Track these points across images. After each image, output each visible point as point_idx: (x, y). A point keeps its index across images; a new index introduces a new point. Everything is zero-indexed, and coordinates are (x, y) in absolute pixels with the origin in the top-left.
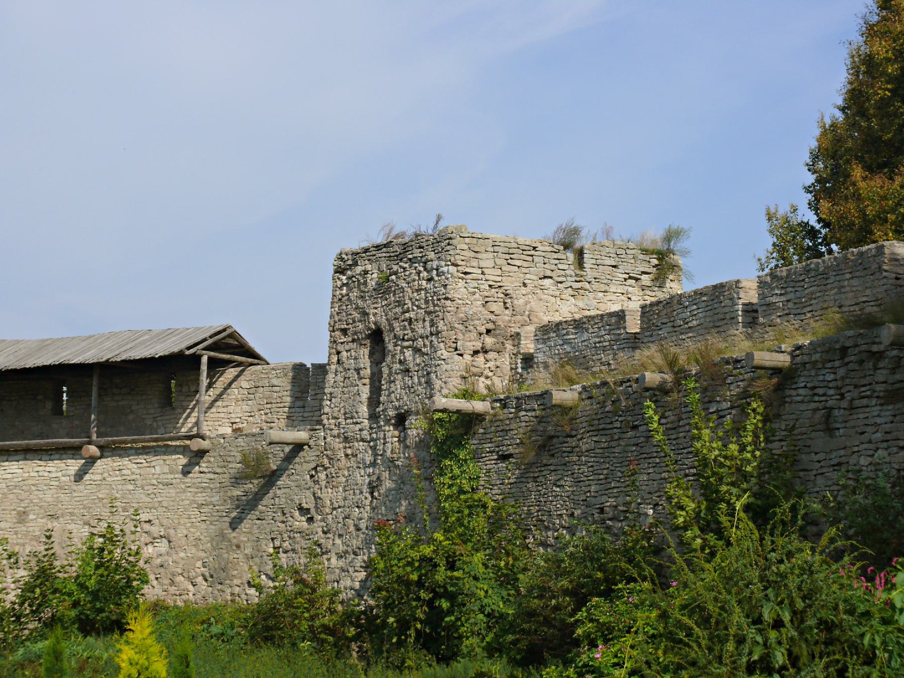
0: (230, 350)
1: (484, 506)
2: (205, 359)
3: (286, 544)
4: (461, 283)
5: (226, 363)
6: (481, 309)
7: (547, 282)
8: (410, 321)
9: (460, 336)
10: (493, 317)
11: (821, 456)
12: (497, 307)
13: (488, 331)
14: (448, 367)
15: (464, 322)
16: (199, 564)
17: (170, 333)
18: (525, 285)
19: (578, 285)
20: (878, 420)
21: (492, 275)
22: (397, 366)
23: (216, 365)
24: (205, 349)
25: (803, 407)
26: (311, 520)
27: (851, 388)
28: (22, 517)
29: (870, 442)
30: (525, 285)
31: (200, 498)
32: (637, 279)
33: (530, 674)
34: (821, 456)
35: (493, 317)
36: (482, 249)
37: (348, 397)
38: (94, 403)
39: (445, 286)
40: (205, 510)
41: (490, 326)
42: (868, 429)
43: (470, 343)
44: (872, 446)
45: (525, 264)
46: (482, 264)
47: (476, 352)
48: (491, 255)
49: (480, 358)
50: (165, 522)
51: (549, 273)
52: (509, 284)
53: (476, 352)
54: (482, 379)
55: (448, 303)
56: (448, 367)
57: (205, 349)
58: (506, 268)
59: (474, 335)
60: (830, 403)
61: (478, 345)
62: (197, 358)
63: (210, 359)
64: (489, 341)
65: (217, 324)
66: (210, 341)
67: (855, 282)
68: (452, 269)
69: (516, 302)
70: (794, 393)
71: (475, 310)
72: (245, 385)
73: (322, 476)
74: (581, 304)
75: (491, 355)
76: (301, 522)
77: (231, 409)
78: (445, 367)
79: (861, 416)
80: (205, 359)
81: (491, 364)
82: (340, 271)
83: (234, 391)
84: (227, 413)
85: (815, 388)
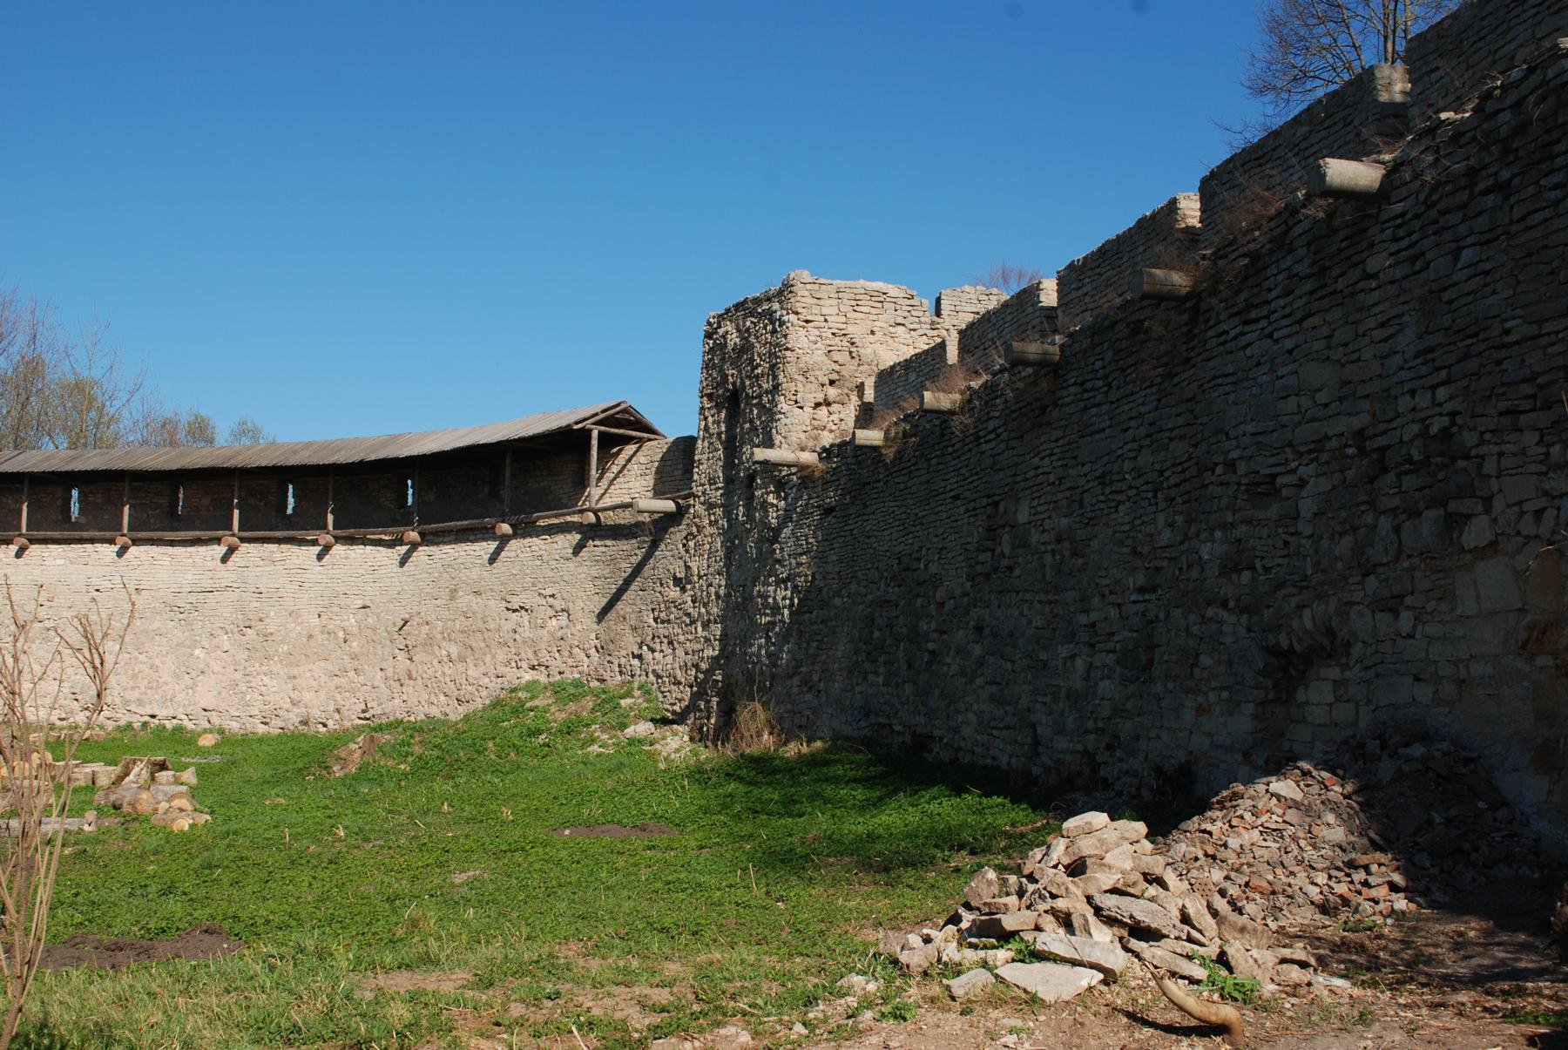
0: (623, 428)
2: (595, 434)
3: (663, 615)
4: (802, 332)
5: (627, 440)
6: (824, 358)
8: (757, 377)
9: (800, 387)
10: (837, 367)
12: (843, 357)
13: (832, 383)
14: (788, 421)
15: (804, 374)
16: (593, 636)
18: (873, 333)
20: (1143, 409)
21: (836, 321)
22: (747, 426)
23: (610, 444)
24: (596, 423)
26: (683, 590)
27: (1117, 374)
30: (873, 333)
35: (837, 367)
36: (824, 295)
37: (709, 463)
39: (785, 336)
41: (834, 377)
42: (1133, 423)
43: (810, 394)
44: (1135, 445)
45: (874, 311)
46: (825, 311)
47: (818, 405)
48: (835, 302)
49: (824, 410)
50: (566, 595)
51: (900, 320)
53: (818, 405)
54: (826, 433)
55: (788, 353)
56: (788, 421)
57: (596, 423)
58: (851, 315)
61: (820, 398)
62: (587, 433)
63: (601, 434)
64: (832, 392)
66: (602, 416)
68: (792, 317)
69: (862, 351)
70: (1065, 393)
71: (815, 358)
72: (643, 460)
73: (691, 544)
75: (834, 407)
76: (674, 593)
77: (631, 485)
78: (784, 421)
79: (1126, 408)
80: (595, 434)
81: (835, 417)
82: (709, 336)
83: (634, 468)
84: (628, 485)
85: (1084, 382)
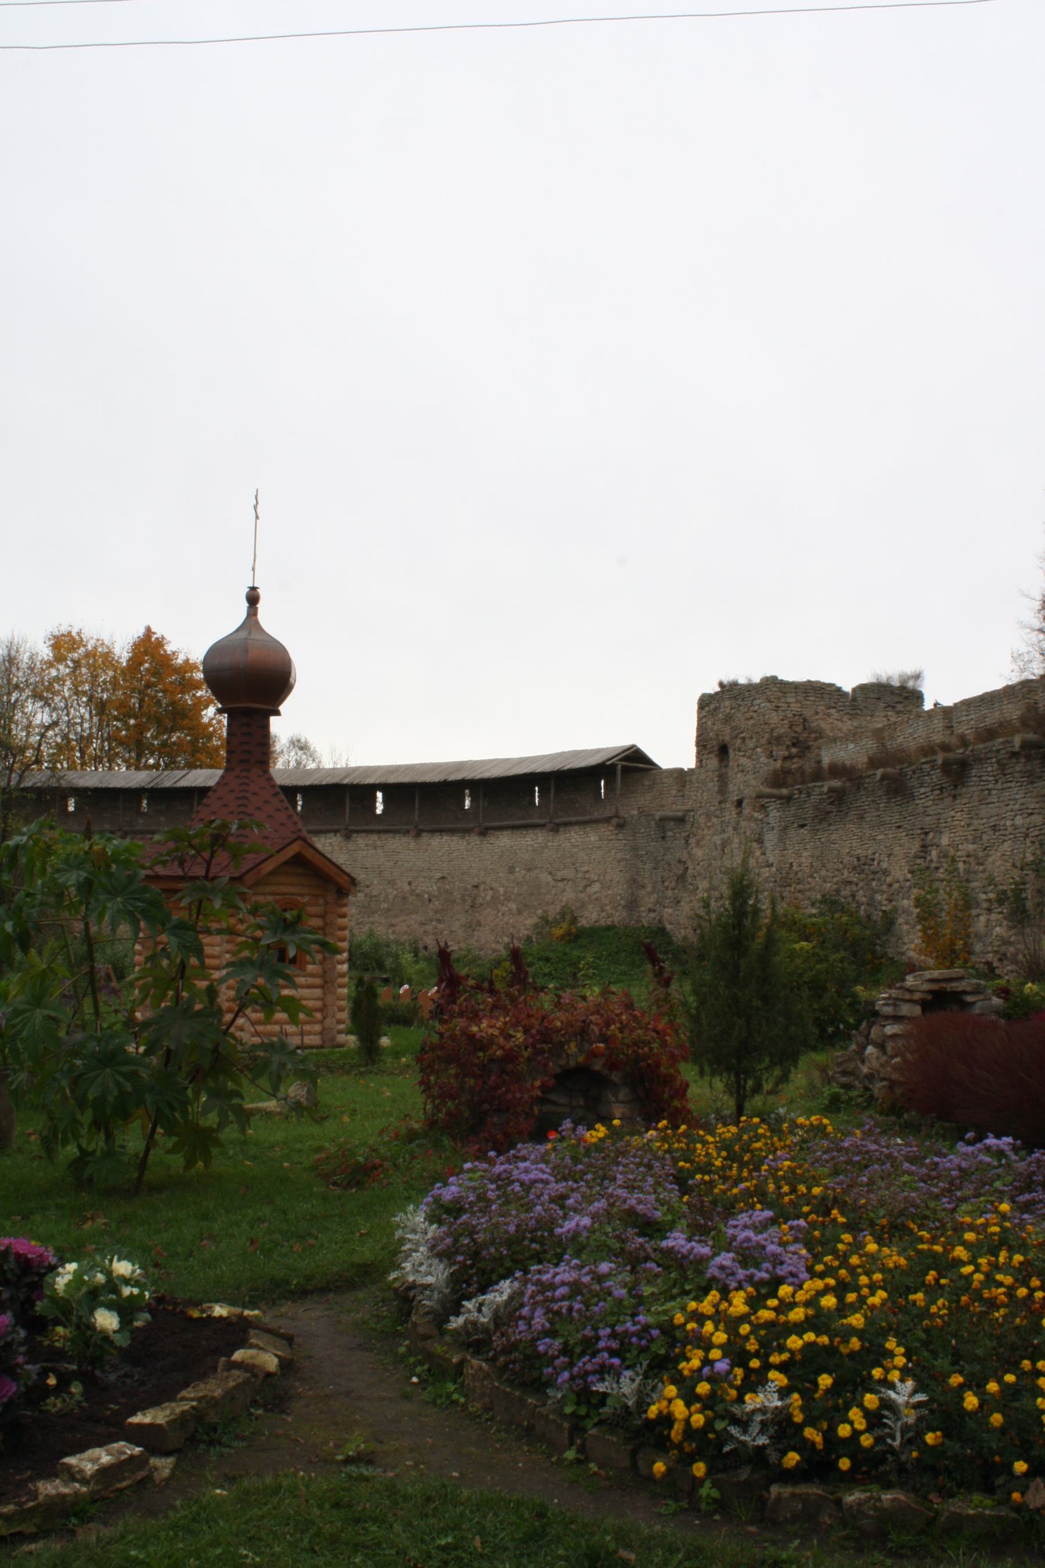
1: (767, 816)
7: (833, 711)
11: (983, 821)
17: (598, 751)
19: (853, 712)
20: (1017, 797)
24: (620, 760)
25: (975, 789)
28: (511, 870)
29: (1012, 811)
31: (619, 856)
32: (894, 707)
33: (1023, 1563)
34: (983, 821)
38: (552, 797)
40: (623, 863)
41: (795, 741)
42: (1011, 802)
51: (833, 705)
52: (807, 713)
59: (784, 747)
60: (990, 787)
61: (786, 753)
63: (623, 767)
64: (794, 750)
65: (626, 742)
67: (1010, 706)
74: (855, 724)
